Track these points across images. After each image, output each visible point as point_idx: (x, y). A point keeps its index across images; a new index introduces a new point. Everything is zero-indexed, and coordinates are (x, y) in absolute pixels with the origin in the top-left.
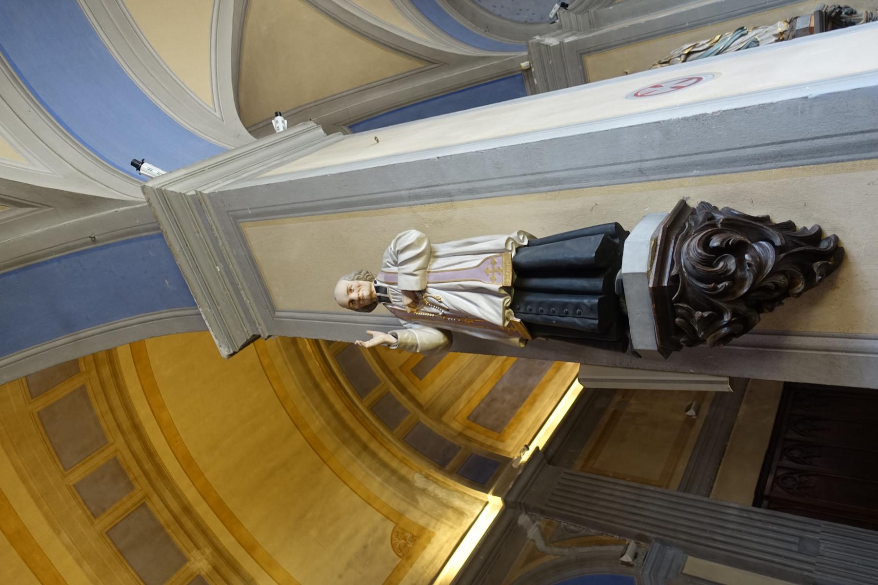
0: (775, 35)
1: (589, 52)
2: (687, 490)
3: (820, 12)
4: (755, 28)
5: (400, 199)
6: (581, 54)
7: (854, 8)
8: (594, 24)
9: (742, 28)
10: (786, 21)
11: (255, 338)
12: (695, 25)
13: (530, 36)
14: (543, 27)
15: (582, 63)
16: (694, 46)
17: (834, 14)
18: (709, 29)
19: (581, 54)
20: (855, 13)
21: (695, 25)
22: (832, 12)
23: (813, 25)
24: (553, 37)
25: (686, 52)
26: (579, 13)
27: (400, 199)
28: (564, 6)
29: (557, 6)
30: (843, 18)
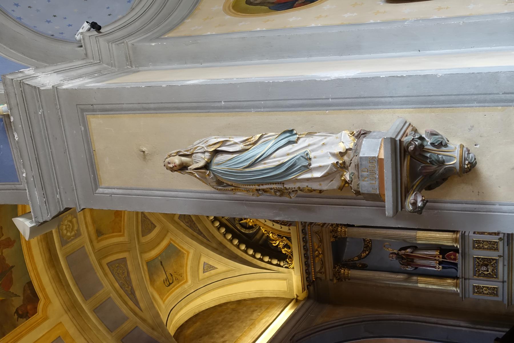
0: (334, 155)
1: (87, 110)
2: (456, 265)
3: (393, 141)
4: (310, 134)
5: (122, 110)
6: (83, 111)
7: (445, 136)
8: (133, 62)
9: (291, 131)
10: (352, 133)
11: (161, 262)
12: (234, 108)
13: (17, 68)
14: (67, 48)
15: (85, 123)
16: (223, 143)
17: (411, 148)
18: (252, 118)
19: (83, 111)
20: (446, 146)
21: (234, 108)
22: (410, 143)
23: (382, 156)
24: (57, 72)
25: (212, 149)
26: (114, 41)
27: (122, 110)
28: (95, 26)
29: (86, 26)
30: (428, 151)
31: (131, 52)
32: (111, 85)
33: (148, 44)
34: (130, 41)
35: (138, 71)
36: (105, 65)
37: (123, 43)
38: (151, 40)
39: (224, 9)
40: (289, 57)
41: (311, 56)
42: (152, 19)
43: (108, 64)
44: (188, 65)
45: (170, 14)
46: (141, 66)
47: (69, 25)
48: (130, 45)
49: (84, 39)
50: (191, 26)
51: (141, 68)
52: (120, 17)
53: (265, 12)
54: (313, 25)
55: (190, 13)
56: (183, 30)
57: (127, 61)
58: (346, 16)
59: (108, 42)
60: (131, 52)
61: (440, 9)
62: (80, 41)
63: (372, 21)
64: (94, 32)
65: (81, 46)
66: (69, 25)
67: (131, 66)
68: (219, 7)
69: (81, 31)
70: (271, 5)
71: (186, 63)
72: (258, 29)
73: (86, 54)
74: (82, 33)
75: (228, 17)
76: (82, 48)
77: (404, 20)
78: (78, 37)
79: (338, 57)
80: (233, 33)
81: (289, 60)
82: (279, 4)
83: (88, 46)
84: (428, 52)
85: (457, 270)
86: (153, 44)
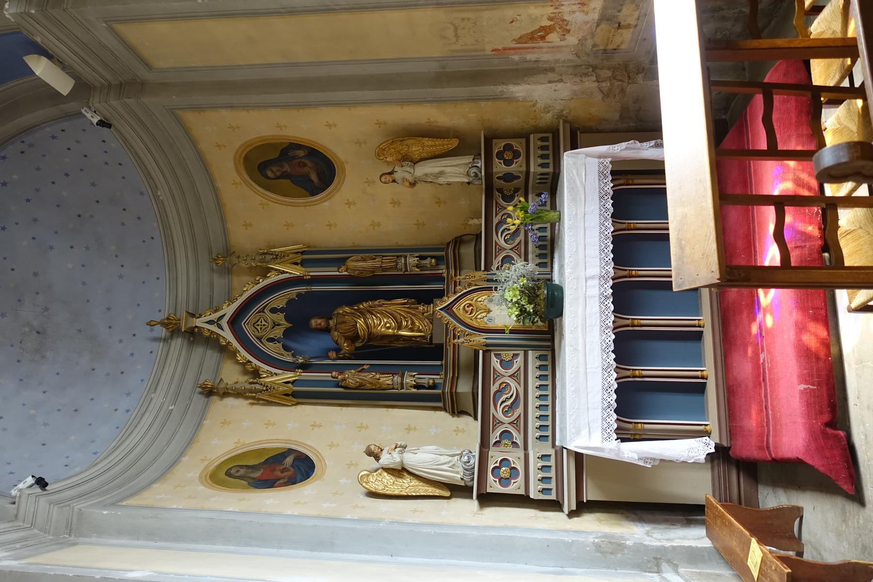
28: (41, 483)
29: (30, 480)
31: (75, 518)
32: (31, 567)
33: (98, 511)
34: (77, 506)
35: (75, 544)
36: (36, 531)
37: (69, 505)
38: (105, 506)
39: (200, 478)
40: (257, 546)
41: (281, 548)
42: (116, 478)
43: (40, 530)
44: (140, 542)
45: (137, 475)
46: (82, 536)
47: (11, 473)
48: (76, 509)
49: (20, 497)
50: (157, 495)
51: (81, 539)
52: (78, 470)
53: (243, 488)
54: (289, 513)
55: (160, 477)
56: (147, 498)
57: (67, 527)
58: (325, 505)
59: (51, 503)
60: (75, 518)
61: (415, 511)
62: (15, 497)
63: (349, 517)
64: (37, 490)
65: (14, 503)
66: (11, 473)
67: (70, 535)
68: (195, 474)
69: (21, 486)
70: (251, 481)
71: (138, 539)
72: (231, 509)
73: (16, 516)
74: (20, 490)
75: (201, 488)
76: (14, 506)
77: (380, 520)
78: (14, 492)
79: (309, 553)
80: (202, 510)
81: (256, 549)
82: (260, 480)
83: (23, 506)
84: (400, 558)
85: (737, 94)
86: (105, 512)
